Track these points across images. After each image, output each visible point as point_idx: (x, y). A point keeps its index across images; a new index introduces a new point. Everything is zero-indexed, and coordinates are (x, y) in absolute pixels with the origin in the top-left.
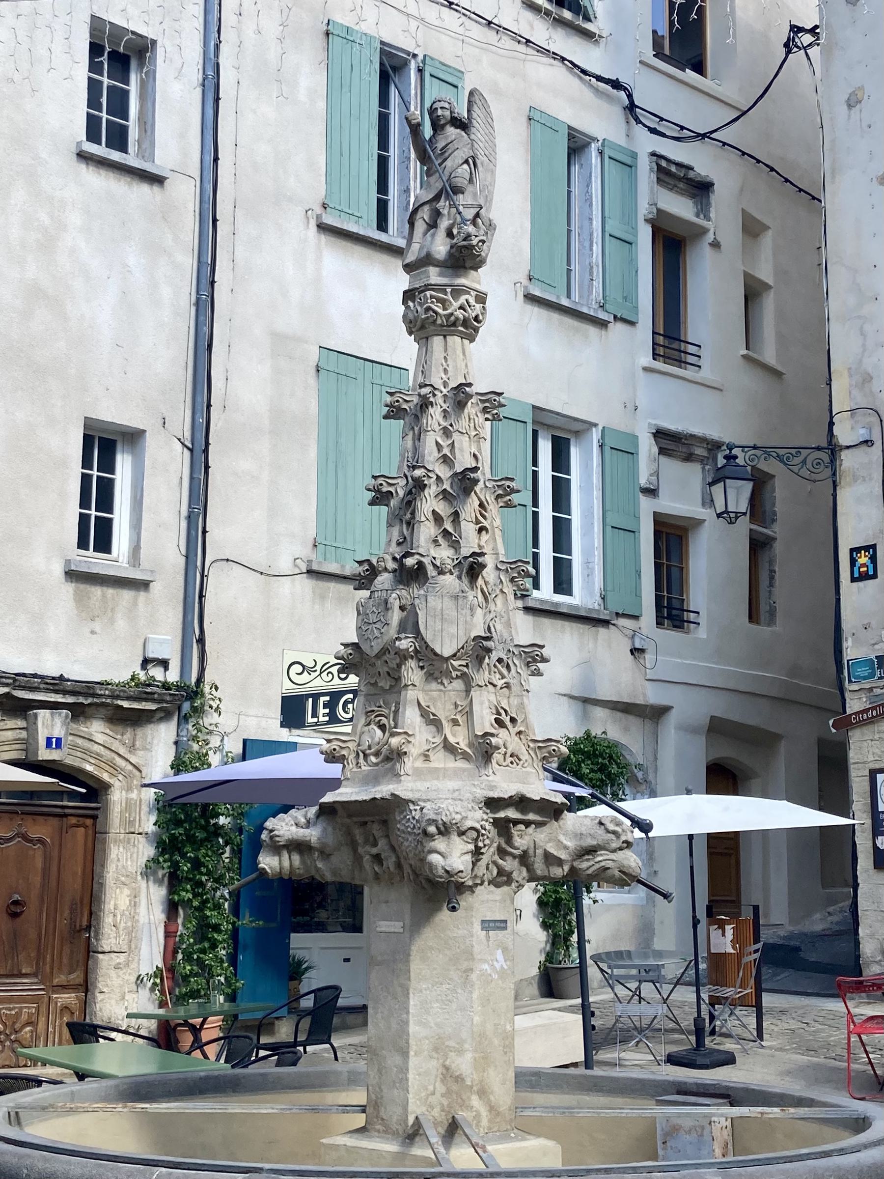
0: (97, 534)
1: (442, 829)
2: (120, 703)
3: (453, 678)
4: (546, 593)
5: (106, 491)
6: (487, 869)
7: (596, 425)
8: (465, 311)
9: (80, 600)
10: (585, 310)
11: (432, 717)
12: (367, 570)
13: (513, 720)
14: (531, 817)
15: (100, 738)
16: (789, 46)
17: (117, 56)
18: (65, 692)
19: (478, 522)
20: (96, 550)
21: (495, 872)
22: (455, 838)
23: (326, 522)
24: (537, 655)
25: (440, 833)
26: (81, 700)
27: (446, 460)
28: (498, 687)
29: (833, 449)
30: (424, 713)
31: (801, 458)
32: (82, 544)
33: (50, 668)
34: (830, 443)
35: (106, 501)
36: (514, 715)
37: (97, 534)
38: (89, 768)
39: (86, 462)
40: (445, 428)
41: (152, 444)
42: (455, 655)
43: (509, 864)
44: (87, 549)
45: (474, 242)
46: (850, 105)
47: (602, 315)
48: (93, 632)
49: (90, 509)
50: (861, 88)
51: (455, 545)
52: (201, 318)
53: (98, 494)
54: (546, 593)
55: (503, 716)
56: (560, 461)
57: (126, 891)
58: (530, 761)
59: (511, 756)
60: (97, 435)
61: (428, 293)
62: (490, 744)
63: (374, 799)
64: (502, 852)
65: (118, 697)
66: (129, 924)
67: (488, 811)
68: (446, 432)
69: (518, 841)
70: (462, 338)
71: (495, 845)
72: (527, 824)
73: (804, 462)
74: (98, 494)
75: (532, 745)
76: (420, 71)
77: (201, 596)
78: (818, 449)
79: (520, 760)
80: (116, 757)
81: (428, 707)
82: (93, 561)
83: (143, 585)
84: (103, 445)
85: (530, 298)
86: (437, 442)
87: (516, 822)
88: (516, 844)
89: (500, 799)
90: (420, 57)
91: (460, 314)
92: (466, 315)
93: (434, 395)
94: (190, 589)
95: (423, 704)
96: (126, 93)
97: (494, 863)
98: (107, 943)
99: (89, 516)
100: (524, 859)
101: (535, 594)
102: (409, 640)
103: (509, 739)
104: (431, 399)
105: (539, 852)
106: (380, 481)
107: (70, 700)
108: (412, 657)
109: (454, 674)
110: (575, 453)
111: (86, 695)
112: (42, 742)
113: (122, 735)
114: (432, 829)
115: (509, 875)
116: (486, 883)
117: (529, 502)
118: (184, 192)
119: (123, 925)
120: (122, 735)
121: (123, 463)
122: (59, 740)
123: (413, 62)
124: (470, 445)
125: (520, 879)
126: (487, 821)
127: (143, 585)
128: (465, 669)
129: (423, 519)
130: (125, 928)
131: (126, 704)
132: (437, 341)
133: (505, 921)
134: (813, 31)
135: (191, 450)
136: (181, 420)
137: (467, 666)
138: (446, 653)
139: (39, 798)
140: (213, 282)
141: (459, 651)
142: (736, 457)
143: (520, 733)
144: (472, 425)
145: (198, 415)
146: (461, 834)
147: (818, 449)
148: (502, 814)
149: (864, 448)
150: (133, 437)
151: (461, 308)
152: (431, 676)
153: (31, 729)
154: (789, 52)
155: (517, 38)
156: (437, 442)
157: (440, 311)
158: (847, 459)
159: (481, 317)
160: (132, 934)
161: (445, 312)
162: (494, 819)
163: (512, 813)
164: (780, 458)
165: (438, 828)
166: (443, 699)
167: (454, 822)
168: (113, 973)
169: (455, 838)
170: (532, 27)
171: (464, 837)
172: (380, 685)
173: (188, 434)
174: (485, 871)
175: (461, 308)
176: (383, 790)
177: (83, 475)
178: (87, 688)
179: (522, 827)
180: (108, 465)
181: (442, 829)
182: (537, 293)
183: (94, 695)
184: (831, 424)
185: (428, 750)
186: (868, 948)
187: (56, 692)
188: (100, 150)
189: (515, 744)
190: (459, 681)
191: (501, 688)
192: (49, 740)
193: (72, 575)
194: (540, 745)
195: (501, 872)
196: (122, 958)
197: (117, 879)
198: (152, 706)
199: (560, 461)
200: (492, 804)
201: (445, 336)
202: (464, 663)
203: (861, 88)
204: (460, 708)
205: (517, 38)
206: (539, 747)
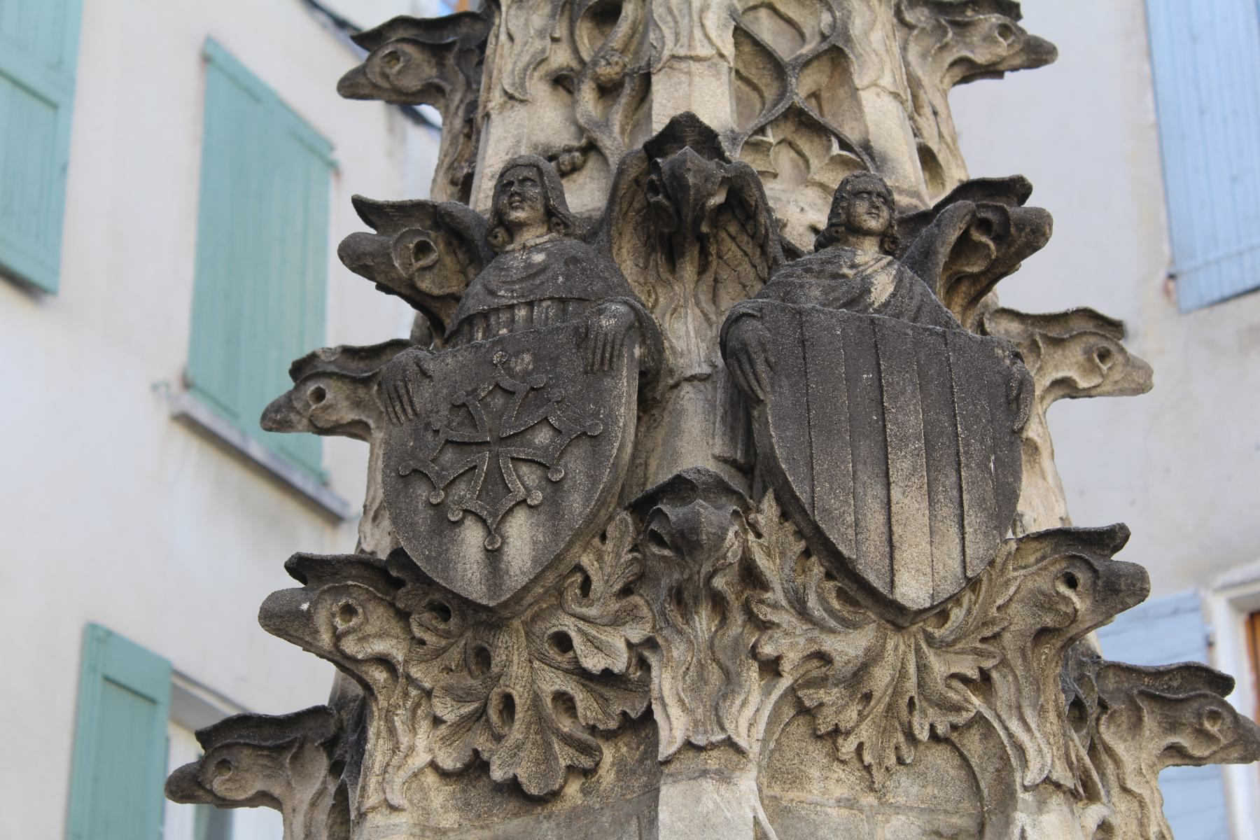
85: (187, 421)
137: (984, 683)
182: (203, 414)
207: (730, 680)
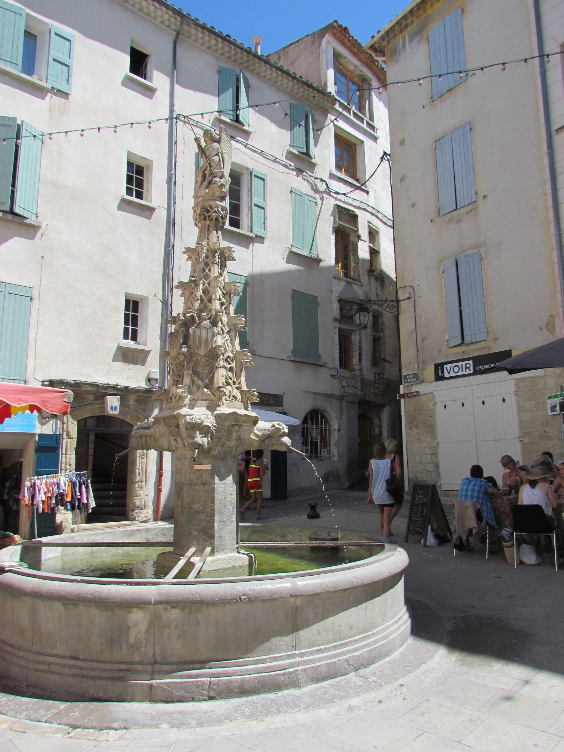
16: (382, 158)
23: (355, 280)
29: (398, 301)
31: (386, 304)
32: (126, 337)
34: (397, 299)
46: (401, 181)
49: (129, 311)
50: (405, 174)
55: (229, 380)
60: (131, 299)
73: (387, 306)
78: (393, 301)
82: (130, 343)
84: (133, 307)
99: (129, 328)
112: (109, 408)
118: (161, 215)
122: (116, 407)
134: (389, 155)
139: (172, 174)
142: (363, 304)
147: (393, 301)
149: (408, 300)
154: (382, 161)
158: (403, 305)
164: (379, 305)
172: (510, 463)
184: (397, 292)
188: (134, 199)
192: (112, 407)
203: (405, 174)
207: (190, 361)
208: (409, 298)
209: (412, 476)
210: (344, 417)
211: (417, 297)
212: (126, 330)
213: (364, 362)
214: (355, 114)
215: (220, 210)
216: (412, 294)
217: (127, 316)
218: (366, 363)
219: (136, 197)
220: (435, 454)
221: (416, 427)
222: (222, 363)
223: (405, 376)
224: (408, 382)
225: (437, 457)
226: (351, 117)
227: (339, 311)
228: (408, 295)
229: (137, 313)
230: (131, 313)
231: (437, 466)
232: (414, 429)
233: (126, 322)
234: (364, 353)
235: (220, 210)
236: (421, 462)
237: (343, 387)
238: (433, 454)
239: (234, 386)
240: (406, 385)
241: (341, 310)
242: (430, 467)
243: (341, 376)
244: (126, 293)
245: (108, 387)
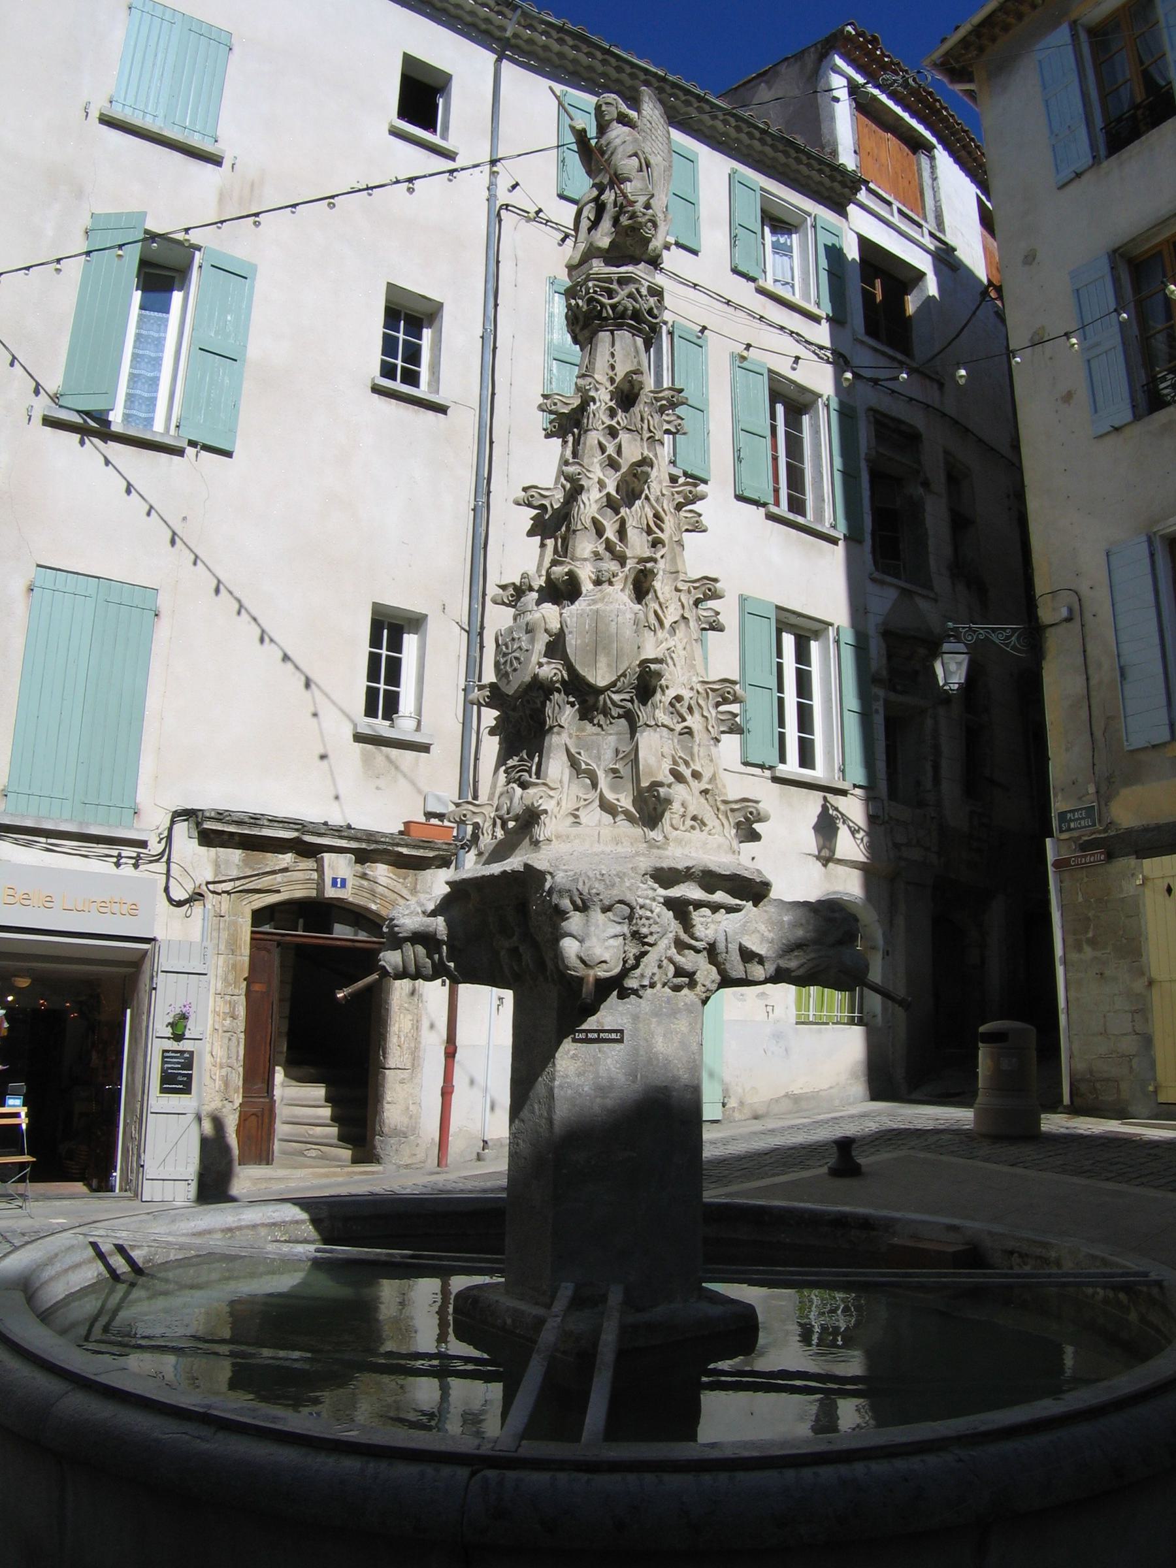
0: (382, 701)
1: (579, 902)
2: (400, 849)
3: (614, 718)
4: (792, 767)
5: (394, 668)
6: (660, 967)
7: (831, 625)
8: (636, 301)
9: (367, 760)
10: (819, 528)
11: (584, 766)
12: (512, 596)
13: (696, 775)
14: (720, 896)
15: (382, 880)
17: (408, 317)
18: (350, 838)
19: (649, 532)
20: (383, 718)
21: (672, 969)
22: (597, 916)
24: (729, 693)
25: (577, 908)
26: (364, 846)
27: (613, 464)
28: (676, 733)
30: (574, 763)
32: (371, 711)
33: (336, 820)
35: (394, 676)
36: (698, 768)
37: (382, 701)
38: (374, 907)
39: (375, 641)
40: (610, 427)
41: (432, 626)
42: (614, 684)
43: (688, 960)
44: (376, 717)
45: (643, 220)
47: (833, 533)
48: (378, 788)
51: (622, 560)
52: (478, 521)
53: (384, 671)
54: (792, 767)
55: (682, 768)
56: (802, 655)
57: (410, 1017)
58: (719, 828)
59: (694, 818)
60: (387, 620)
61: (590, 284)
62: (658, 797)
63: (505, 871)
64: (680, 945)
65: (398, 845)
66: (413, 1045)
67: (656, 886)
68: (613, 432)
69: (699, 931)
70: (634, 335)
71: (671, 935)
72: (715, 908)
74: (384, 671)
75: (722, 807)
76: (671, 333)
77: (476, 759)
79: (705, 825)
80: (399, 898)
81: (579, 754)
82: (380, 726)
83: (425, 748)
84: (390, 628)
86: (600, 443)
87: (699, 905)
88: (698, 934)
89: (673, 871)
90: (670, 323)
91: (629, 304)
92: (637, 306)
93: (597, 390)
94: (466, 752)
95: (573, 751)
96: (419, 347)
97: (671, 960)
98: (391, 1062)
99: (380, 655)
100: (712, 951)
101: (781, 766)
102: (553, 666)
103: (689, 798)
104: (592, 393)
105: (734, 948)
106: (532, 492)
107: (354, 845)
108: (559, 691)
109: (615, 714)
110: (814, 646)
111: (368, 841)
113: (405, 879)
114: (566, 903)
115: (691, 975)
116: (659, 986)
117: (775, 686)
118: (464, 420)
119: (406, 1045)
120: (405, 879)
121: (410, 641)
122: (344, 881)
123: (664, 327)
124: (642, 447)
125: (707, 983)
126: (654, 899)
127: (425, 748)
128: (629, 705)
129: (579, 527)
130: (409, 1048)
131: (405, 851)
132: (604, 336)
133: (621, 1032)
135: (468, 632)
136: (460, 608)
137: (632, 701)
138: (601, 682)
140: (489, 492)
141: (618, 679)
143: (705, 792)
144: (645, 426)
145: (474, 601)
146: (606, 909)
148: (676, 892)
149: (1065, 624)
150: (416, 623)
151: (630, 296)
152: (586, 714)
153: (320, 870)
155: (751, 314)
156: (600, 443)
157: (605, 301)
159: (655, 311)
160: (415, 1054)
161: (611, 301)
162: (665, 897)
163: (692, 891)
165: (573, 902)
166: (604, 743)
167: (594, 891)
168: (398, 1087)
169: (597, 916)
170: (764, 307)
171: (609, 914)
173: (465, 619)
174: (656, 970)
175: (630, 296)
176: (514, 863)
177: (371, 654)
178: (370, 836)
179: (706, 911)
180: (396, 645)
181: (579, 902)
183: (377, 842)
185: (577, 810)
186: (1164, 1073)
187: (341, 837)
189: (697, 805)
190: (623, 720)
191: (681, 734)
192: (334, 881)
193: (359, 738)
194: (735, 806)
195: (679, 972)
196: (405, 1075)
197: (401, 1006)
198: (431, 854)
199: (802, 655)
200: (665, 877)
201: (612, 332)
202: (627, 696)
204: (621, 756)
205: (751, 314)
206: (732, 810)
208: (1069, 619)
209: (1080, 1066)
210: (900, 921)
211: (1088, 616)
212: (372, 694)
213: (945, 786)
214: (900, 211)
215: (644, 291)
216: (1076, 607)
217: (374, 660)
218: (950, 789)
219: (403, 381)
220: (1142, 1011)
221: (1093, 943)
222: (662, 716)
223: (1062, 816)
224: (1069, 829)
225: (1147, 1020)
226: (896, 219)
227: (884, 661)
228: (1064, 612)
229: (398, 686)
230: (382, 686)
231: (1147, 1041)
232: (1087, 949)
233: (373, 675)
234: (944, 763)
235: (644, 291)
236: (1104, 1033)
237: (897, 846)
238: (1136, 1012)
239: (696, 786)
240: (1065, 836)
241: (890, 657)
242: (1129, 1045)
243: (890, 818)
244: (391, 287)
245: (327, 829)
